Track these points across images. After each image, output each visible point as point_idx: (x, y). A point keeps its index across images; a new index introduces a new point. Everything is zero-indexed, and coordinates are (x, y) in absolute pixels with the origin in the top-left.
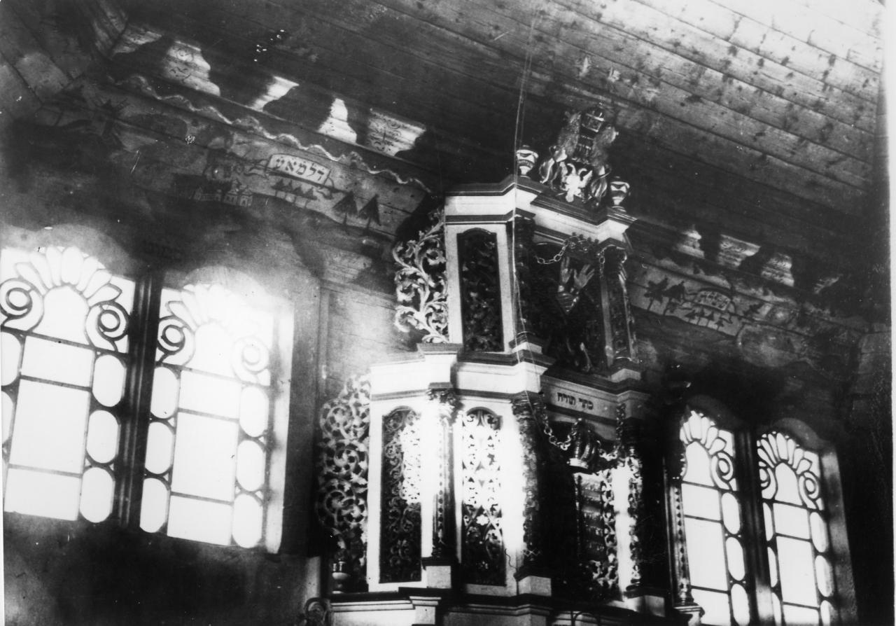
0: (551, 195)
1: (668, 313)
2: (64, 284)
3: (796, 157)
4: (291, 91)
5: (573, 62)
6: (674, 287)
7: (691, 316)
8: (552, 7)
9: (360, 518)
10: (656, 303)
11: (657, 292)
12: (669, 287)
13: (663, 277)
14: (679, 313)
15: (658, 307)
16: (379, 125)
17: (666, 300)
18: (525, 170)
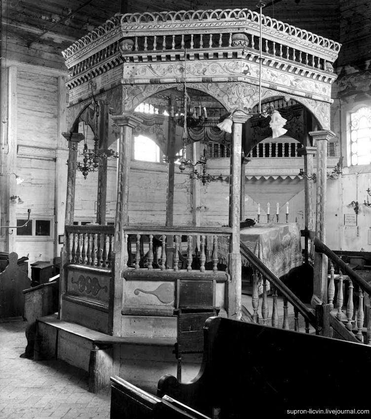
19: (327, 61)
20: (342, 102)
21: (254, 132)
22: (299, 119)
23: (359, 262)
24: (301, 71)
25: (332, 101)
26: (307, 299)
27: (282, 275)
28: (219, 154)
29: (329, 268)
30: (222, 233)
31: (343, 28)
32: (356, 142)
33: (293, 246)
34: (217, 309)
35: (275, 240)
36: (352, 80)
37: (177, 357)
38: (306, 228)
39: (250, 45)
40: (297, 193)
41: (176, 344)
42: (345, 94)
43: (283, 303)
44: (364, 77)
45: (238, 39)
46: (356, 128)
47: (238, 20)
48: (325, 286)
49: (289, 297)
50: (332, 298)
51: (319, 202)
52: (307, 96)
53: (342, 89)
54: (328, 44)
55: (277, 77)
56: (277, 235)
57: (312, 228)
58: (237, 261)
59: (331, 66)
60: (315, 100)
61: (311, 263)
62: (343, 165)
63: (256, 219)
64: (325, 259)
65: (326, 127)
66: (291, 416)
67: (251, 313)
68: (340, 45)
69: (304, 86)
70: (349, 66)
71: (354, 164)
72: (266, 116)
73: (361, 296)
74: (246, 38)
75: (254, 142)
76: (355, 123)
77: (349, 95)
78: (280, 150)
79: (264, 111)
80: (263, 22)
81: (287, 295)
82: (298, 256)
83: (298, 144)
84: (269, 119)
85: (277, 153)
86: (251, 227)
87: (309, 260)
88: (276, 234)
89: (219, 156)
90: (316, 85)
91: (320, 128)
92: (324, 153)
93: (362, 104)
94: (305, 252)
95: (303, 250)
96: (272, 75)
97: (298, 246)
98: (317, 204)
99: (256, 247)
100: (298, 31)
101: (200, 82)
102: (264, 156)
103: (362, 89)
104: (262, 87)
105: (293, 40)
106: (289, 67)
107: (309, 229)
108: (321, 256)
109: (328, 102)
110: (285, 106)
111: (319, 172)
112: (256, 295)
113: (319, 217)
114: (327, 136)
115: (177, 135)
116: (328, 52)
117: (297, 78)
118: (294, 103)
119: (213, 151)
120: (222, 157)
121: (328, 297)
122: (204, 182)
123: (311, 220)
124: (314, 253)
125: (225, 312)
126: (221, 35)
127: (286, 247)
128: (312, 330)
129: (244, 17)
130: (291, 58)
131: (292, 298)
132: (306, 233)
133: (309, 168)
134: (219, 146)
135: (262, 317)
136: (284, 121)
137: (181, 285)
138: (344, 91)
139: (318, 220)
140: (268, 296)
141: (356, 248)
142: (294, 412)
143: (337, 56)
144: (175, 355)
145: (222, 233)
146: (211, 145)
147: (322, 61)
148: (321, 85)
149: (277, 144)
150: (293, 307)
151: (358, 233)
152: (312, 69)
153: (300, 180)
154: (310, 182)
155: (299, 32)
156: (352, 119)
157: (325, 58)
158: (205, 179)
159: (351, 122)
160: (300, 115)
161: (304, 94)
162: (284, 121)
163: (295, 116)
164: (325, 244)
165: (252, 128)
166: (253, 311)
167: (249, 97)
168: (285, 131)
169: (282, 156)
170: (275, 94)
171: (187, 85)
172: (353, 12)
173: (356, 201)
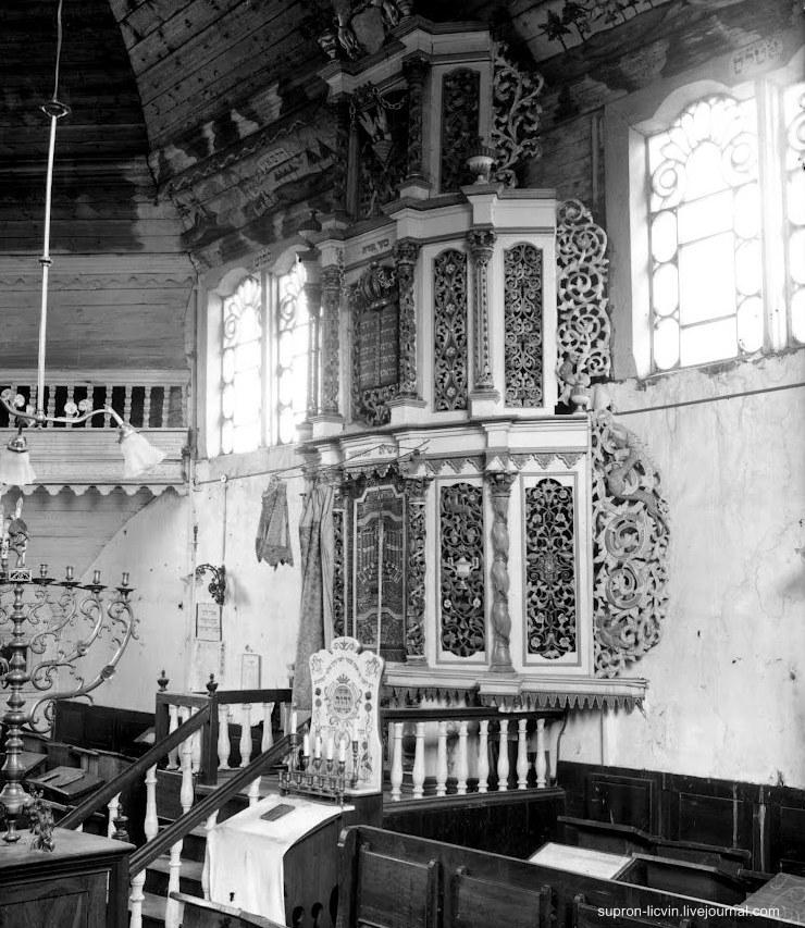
1: (587, 36)
2: (699, 143)
3: (222, 8)
6: (565, 10)
8: (212, 255)
9: (534, 512)
10: (565, 37)
11: (556, 28)
12: (561, 16)
13: (545, 13)
14: (598, 27)
15: (573, 40)
17: (571, 26)
40: (110, 537)
53: (189, 224)
62: (200, 455)
66: (607, 921)
71: (665, 364)
93: (236, 271)
138: (193, 231)
142: (614, 913)
151: (222, 665)
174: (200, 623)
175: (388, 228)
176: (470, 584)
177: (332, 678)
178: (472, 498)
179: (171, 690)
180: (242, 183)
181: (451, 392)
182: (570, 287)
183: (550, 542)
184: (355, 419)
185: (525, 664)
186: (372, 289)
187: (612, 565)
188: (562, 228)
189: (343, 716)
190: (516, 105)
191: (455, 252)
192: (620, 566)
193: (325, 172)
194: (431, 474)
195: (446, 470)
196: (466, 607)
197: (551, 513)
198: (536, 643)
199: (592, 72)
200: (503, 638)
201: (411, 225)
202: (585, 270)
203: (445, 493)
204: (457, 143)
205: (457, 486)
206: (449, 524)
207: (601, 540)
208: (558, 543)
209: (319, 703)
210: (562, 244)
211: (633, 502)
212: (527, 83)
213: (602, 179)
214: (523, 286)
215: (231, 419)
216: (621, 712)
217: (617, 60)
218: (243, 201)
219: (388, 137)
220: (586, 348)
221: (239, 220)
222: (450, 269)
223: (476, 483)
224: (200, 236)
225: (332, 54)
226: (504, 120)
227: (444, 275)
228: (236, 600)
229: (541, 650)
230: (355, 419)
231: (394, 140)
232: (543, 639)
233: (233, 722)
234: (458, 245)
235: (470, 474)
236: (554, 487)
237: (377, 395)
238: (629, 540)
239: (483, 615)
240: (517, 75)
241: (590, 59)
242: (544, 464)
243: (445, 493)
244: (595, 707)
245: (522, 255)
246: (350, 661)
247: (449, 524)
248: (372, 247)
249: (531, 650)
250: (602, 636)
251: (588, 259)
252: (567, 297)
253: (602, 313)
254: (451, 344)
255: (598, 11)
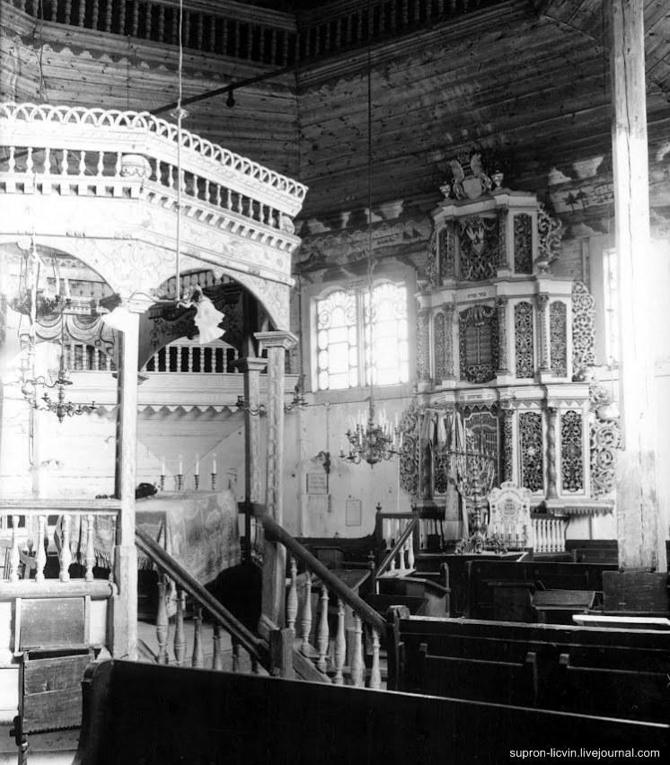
0: (462, 199)
4: (350, 216)
5: (443, 140)
6: (578, 194)
7: (602, 201)
9: (564, 426)
10: (574, 205)
11: (571, 200)
14: (592, 204)
15: (579, 206)
16: (385, 209)
17: (579, 201)
18: (447, 195)
19: (284, 214)
20: (303, 280)
21: (155, 327)
22: (236, 310)
23: (336, 555)
24: (242, 228)
25: (292, 282)
26: (253, 622)
27: (206, 582)
28: (85, 363)
29: (289, 566)
30: (103, 510)
31: (305, 154)
32: (327, 350)
33: (226, 531)
34: (95, 647)
35: (193, 521)
36: (320, 245)
37: (19, 742)
38: (248, 498)
39: (153, 178)
41: (16, 718)
42: (311, 268)
43: (212, 631)
44: (338, 240)
45: (131, 165)
46: (326, 327)
47: (130, 131)
48: (282, 597)
49: (223, 620)
50: (293, 619)
51: (271, 453)
52: (251, 271)
53: (303, 259)
54: (285, 185)
55: (199, 235)
56: (198, 510)
57: (257, 497)
58: (130, 561)
59: (291, 223)
60: (265, 279)
61: (256, 560)
63: (159, 483)
64: (281, 551)
65: (282, 326)
67: (154, 652)
68: (305, 189)
69: (245, 253)
70: (315, 220)
71: (323, 388)
72: (188, 305)
73: (342, 613)
74: (147, 164)
75: (155, 345)
76: (325, 318)
77: (315, 269)
78: (201, 361)
79: (185, 297)
80: (176, 138)
81: (219, 616)
82: (233, 548)
83: (228, 350)
84: (193, 310)
85: (190, 365)
86: (149, 497)
87: (253, 554)
88: (195, 509)
89: (85, 367)
90: (266, 254)
91: (271, 328)
92: (279, 369)
94: (245, 541)
95: (242, 537)
96: (193, 232)
97: (234, 531)
98: (268, 457)
99: (160, 534)
100: (236, 159)
101: (63, 236)
102: (168, 369)
103: (336, 261)
104: (181, 253)
105: (228, 174)
106: (221, 220)
107: (252, 500)
108: (275, 546)
109: (286, 284)
110: (210, 284)
111: (272, 402)
112: (163, 619)
113: (270, 480)
114: (285, 341)
115: (10, 328)
116: (286, 197)
117: (235, 240)
118: (227, 281)
119: (73, 358)
120: (91, 369)
121: (287, 617)
122: (60, 415)
123: (255, 484)
124: (261, 542)
125: (108, 653)
126: (102, 155)
127: (213, 532)
128: (263, 673)
129: (142, 126)
130: (235, 209)
131: (229, 621)
132: (247, 508)
133: (252, 394)
134: (85, 349)
135: (174, 658)
136: (220, 316)
137: (24, 609)
139: (270, 484)
140: (185, 619)
141: (326, 531)
143: (301, 207)
144: (14, 738)
145: (103, 510)
146: (68, 347)
147: (276, 213)
148: (274, 254)
149: (191, 348)
150: (229, 637)
152: (260, 225)
153: (231, 414)
154: (255, 420)
155: (238, 162)
156: (320, 311)
157: (282, 209)
158: (61, 410)
159: (317, 316)
160: (236, 302)
161: (246, 268)
162: (220, 316)
163: (226, 303)
164: (281, 524)
165: (152, 320)
166: (159, 648)
167: (151, 269)
168: (222, 332)
169: (165, 371)
170: (196, 265)
171: (38, 240)
172: (320, 130)
173: (326, 451)
174: (310, 484)
175: (491, 288)
176: (534, 458)
177: (503, 499)
178: (536, 419)
179: (383, 511)
180: (352, 243)
181: (525, 369)
182: (578, 322)
183: (572, 439)
184: (462, 378)
185: (562, 495)
186: (478, 316)
187: (600, 449)
188: (575, 295)
189: (509, 516)
190: (549, 234)
191: (525, 303)
192: (604, 450)
193: (412, 244)
194: (514, 408)
195: (522, 406)
196: (533, 469)
197: (572, 426)
198: (566, 485)
199: (587, 222)
200: (551, 480)
201: (504, 289)
202: (585, 315)
203: (522, 416)
204: (522, 250)
205: (527, 413)
206: (524, 431)
207: (594, 438)
208: (575, 440)
209: (494, 511)
210: (574, 302)
211: (609, 422)
212: (554, 224)
213: (589, 271)
214: (558, 321)
215: (327, 370)
216: (600, 515)
217: (599, 219)
218: (350, 251)
219: (482, 242)
220: (585, 351)
221: (344, 260)
222: (523, 311)
223: (538, 412)
224: (310, 266)
225: (447, 195)
226: (544, 240)
227: (520, 313)
228: (339, 470)
229: (568, 488)
230: (462, 378)
231: (485, 243)
232: (569, 483)
233: (83, 579)
234: (528, 300)
235: (535, 408)
236: (573, 414)
237: (477, 368)
238: (609, 438)
239: (542, 473)
240: (549, 219)
241: (585, 216)
242: (569, 404)
243: (522, 416)
244: (589, 514)
245: (557, 307)
246: (513, 492)
247: (524, 431)
248: (475, 295)
249: (564, 488)
250: (594, 481)
251: (586, 310)
252: (577, 327)
253: (592, 335)
254: (525, 346)
255: (595, 197)
